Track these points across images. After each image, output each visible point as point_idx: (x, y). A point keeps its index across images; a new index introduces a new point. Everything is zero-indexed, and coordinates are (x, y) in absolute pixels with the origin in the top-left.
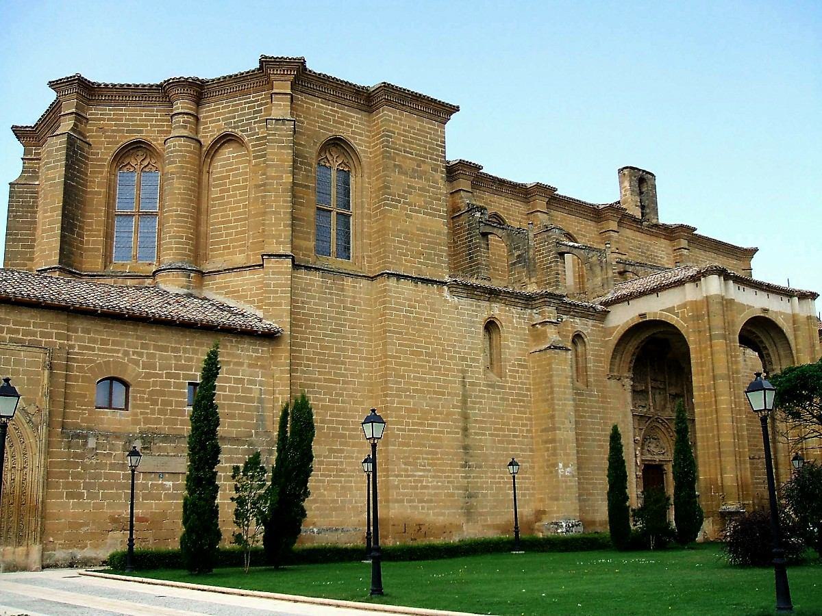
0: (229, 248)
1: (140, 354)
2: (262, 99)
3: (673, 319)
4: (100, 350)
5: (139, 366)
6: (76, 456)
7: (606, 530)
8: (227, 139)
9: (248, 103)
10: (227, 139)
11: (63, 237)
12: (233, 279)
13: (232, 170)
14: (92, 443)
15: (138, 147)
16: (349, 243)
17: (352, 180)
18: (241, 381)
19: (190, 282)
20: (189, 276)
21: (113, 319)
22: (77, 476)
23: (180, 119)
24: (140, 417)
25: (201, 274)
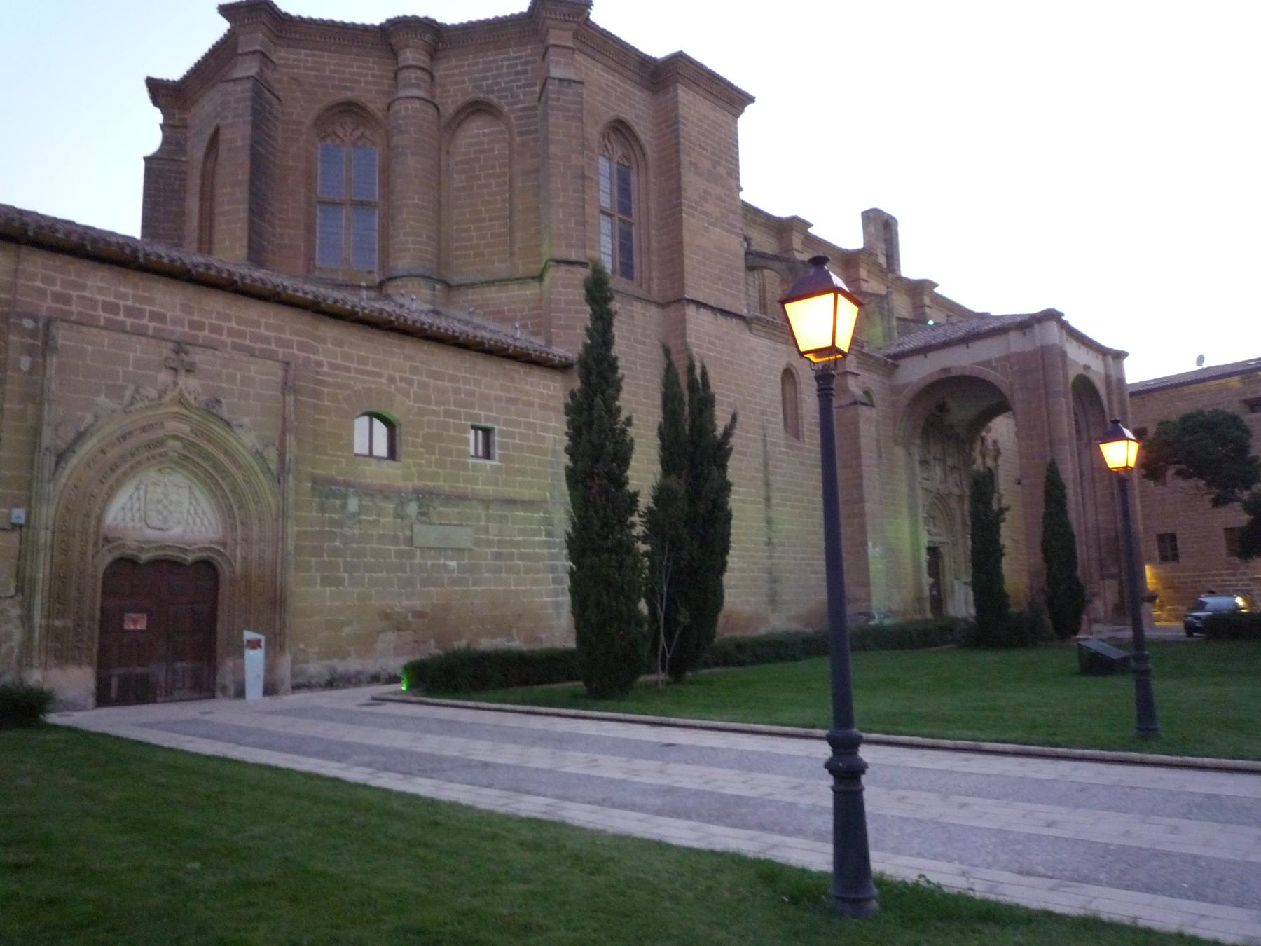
0: (483, 255)
1: (410, 382)
2: (527, 56)
3: (990, 375)
4: (357, 371)
5: (408, 397)
6: (334, 523)
7: (559, 631)
8: (477, 108)
9: (508, 59)
10: (477, 108)
11: (251, 222)
12: (495, 295)
13: (483, 151)
14: (353, 504)
15: (352, 110)
16: (631, 259)
17: (634, 179)
18: (531, 426)
19: (435, 296)
20: (434, 289)
21: (622, 246)
22: (334, 552)
23: (413, 75)
24: (414, 470)
25: (448, 286)
